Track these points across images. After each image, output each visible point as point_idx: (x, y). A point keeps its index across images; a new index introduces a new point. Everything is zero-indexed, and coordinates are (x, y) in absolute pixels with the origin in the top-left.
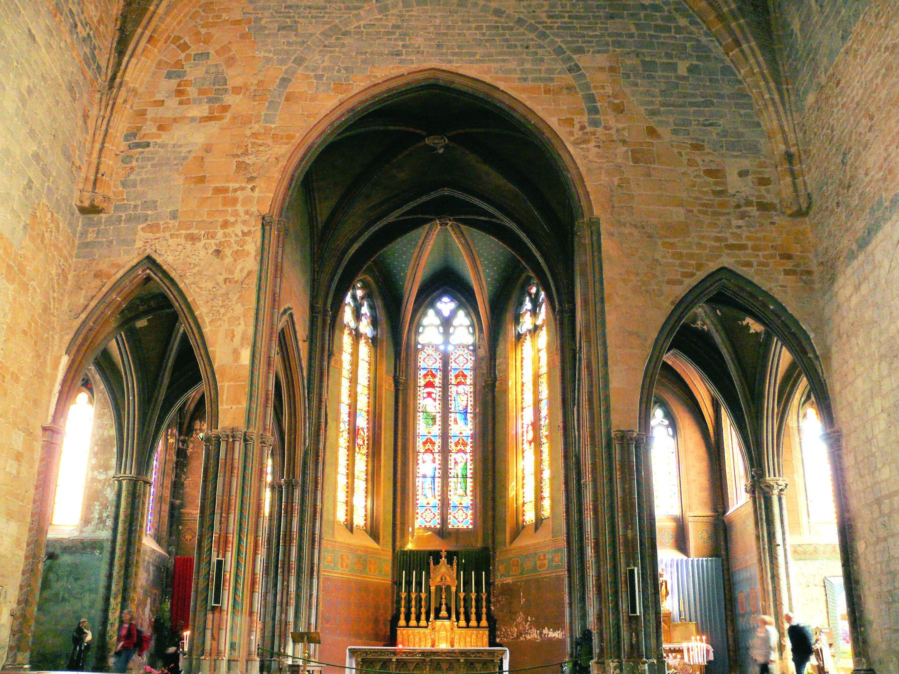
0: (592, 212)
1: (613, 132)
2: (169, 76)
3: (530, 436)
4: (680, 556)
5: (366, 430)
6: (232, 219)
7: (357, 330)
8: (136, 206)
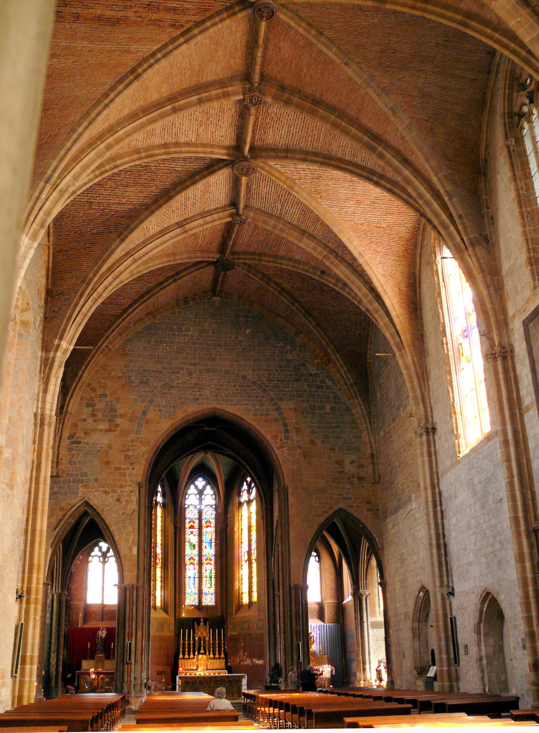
1: (295, 442)
2: (87, 405)
3: (246, 557)
4: (320, 623)
6: (124, 484)
8: (77, 475)
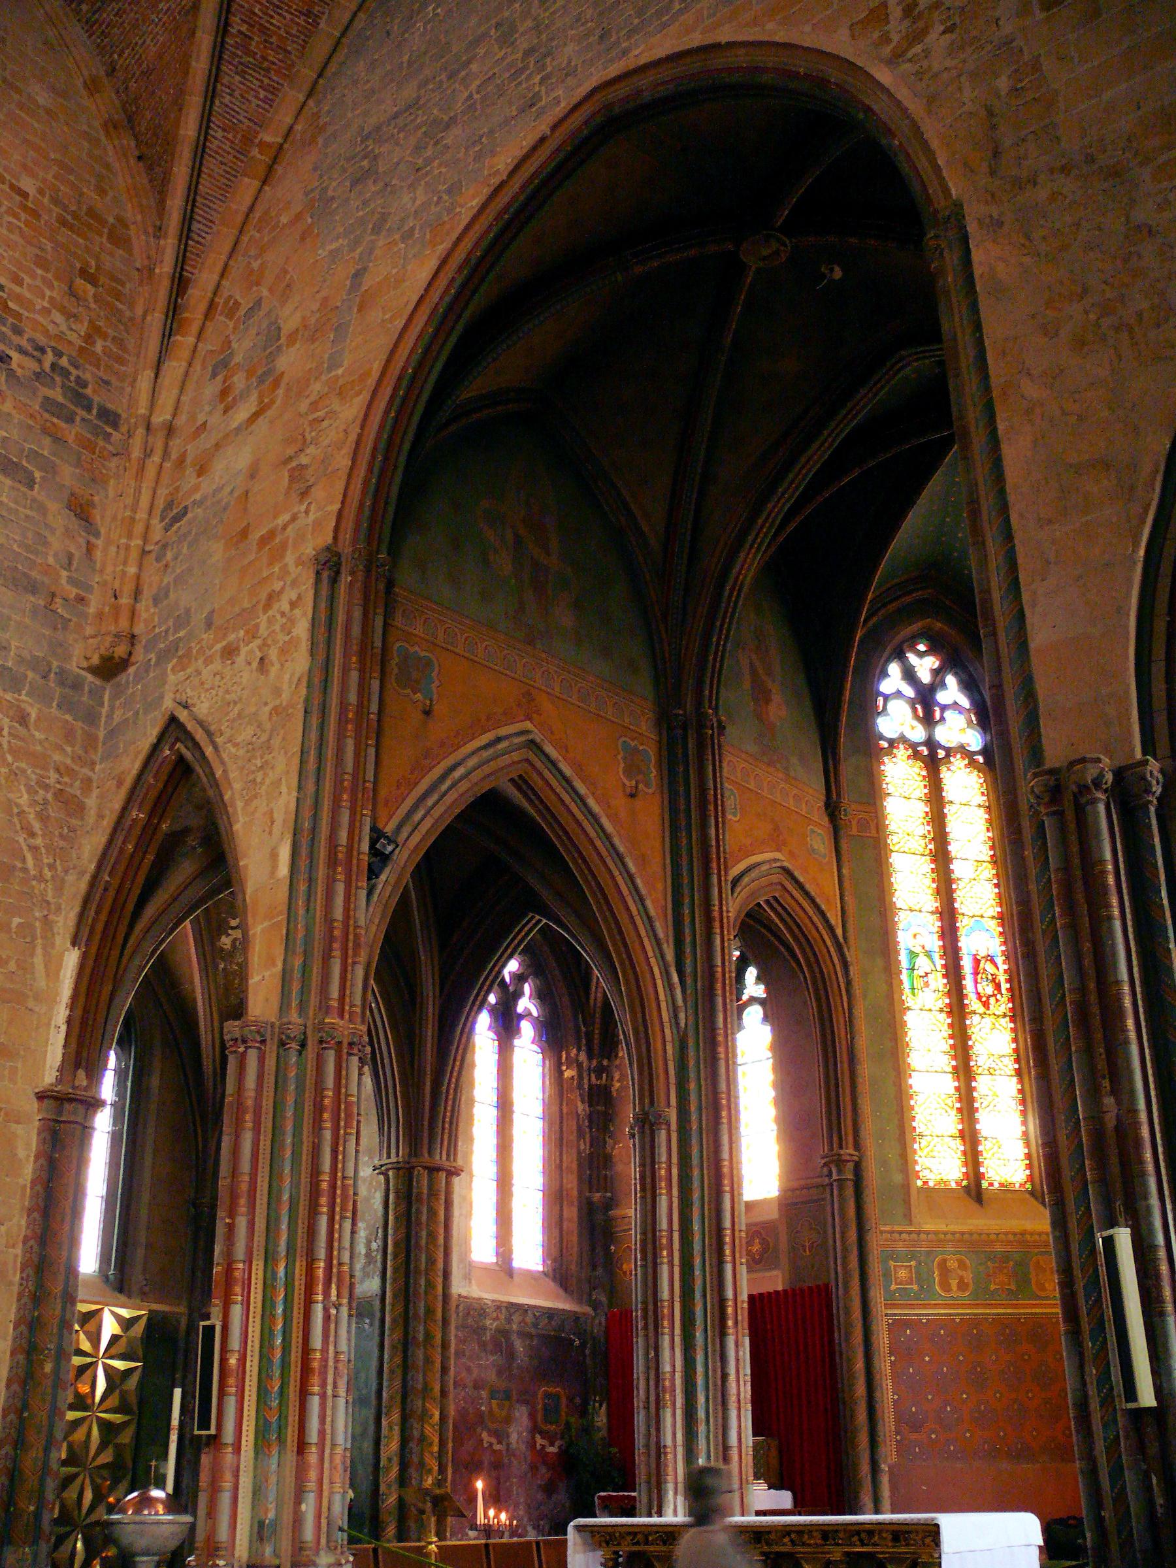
0: (950, 195)
5: (999, 960)
7: (931, 743)
